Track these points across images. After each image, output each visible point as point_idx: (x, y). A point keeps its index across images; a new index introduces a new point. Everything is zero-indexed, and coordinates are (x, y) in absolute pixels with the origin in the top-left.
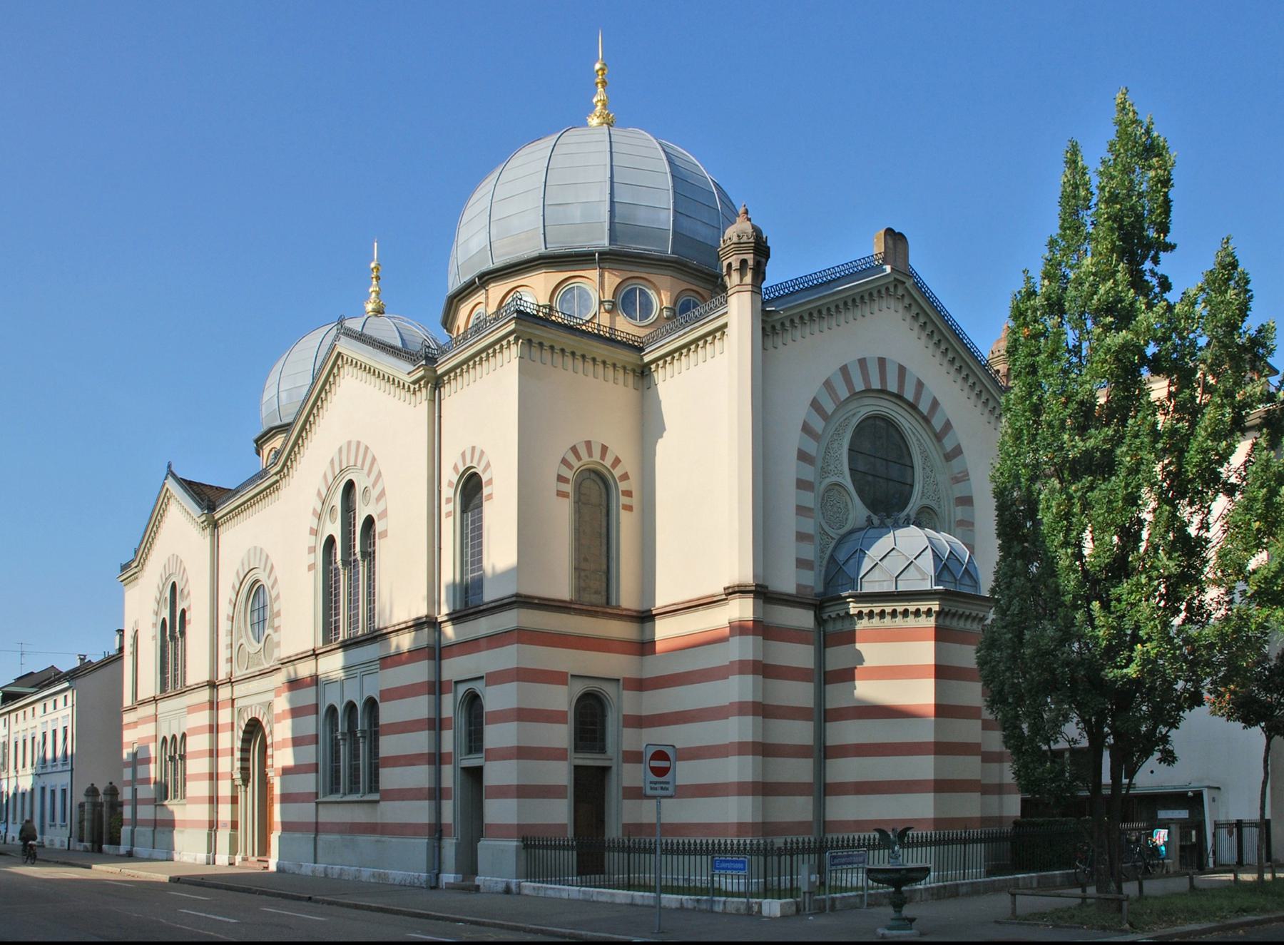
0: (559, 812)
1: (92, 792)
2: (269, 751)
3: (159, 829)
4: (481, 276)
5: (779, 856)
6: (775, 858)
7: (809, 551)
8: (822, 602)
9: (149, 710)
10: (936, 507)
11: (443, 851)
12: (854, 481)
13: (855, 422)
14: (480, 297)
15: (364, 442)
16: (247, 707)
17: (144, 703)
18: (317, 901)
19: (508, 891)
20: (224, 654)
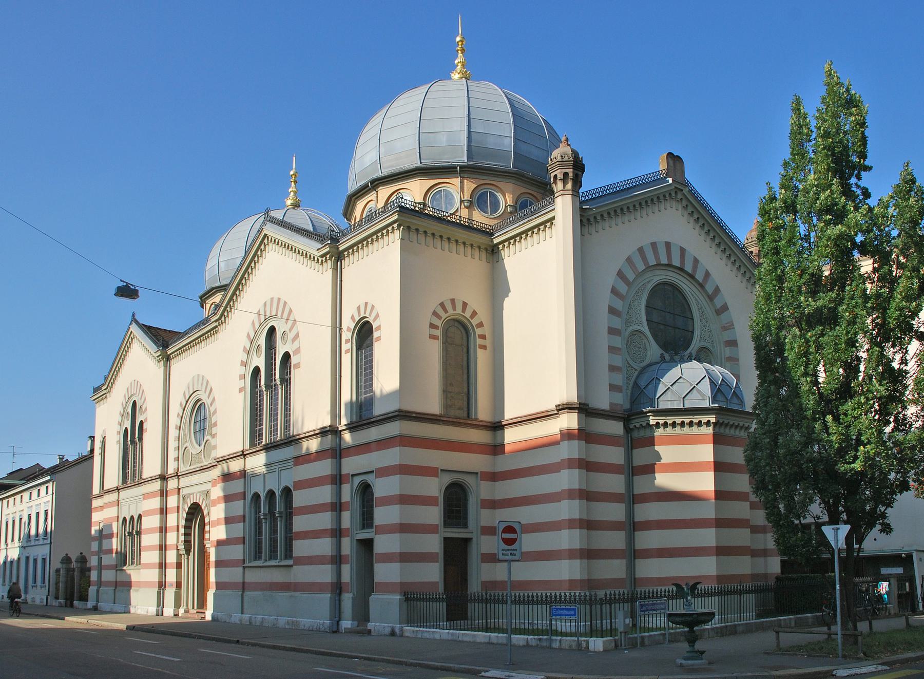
0: (432, 573)
1: (67, 560)
2: (207, 528)
3: (119, 588)
4: (373, 182)
5: (601, 605)
6: (598, 606)
7: (619, 379)
8: (629, 416)
9: (113, 497)
10: (710, 347)
11: (342, 603)
12: (650, 329)
13: (650, 286)
14: (372, 196)
15: (283, 299)
16: (190, 494)
17: (109, 491)
18: (243, 644)
19: (393, 633)
20: (172, 454)
